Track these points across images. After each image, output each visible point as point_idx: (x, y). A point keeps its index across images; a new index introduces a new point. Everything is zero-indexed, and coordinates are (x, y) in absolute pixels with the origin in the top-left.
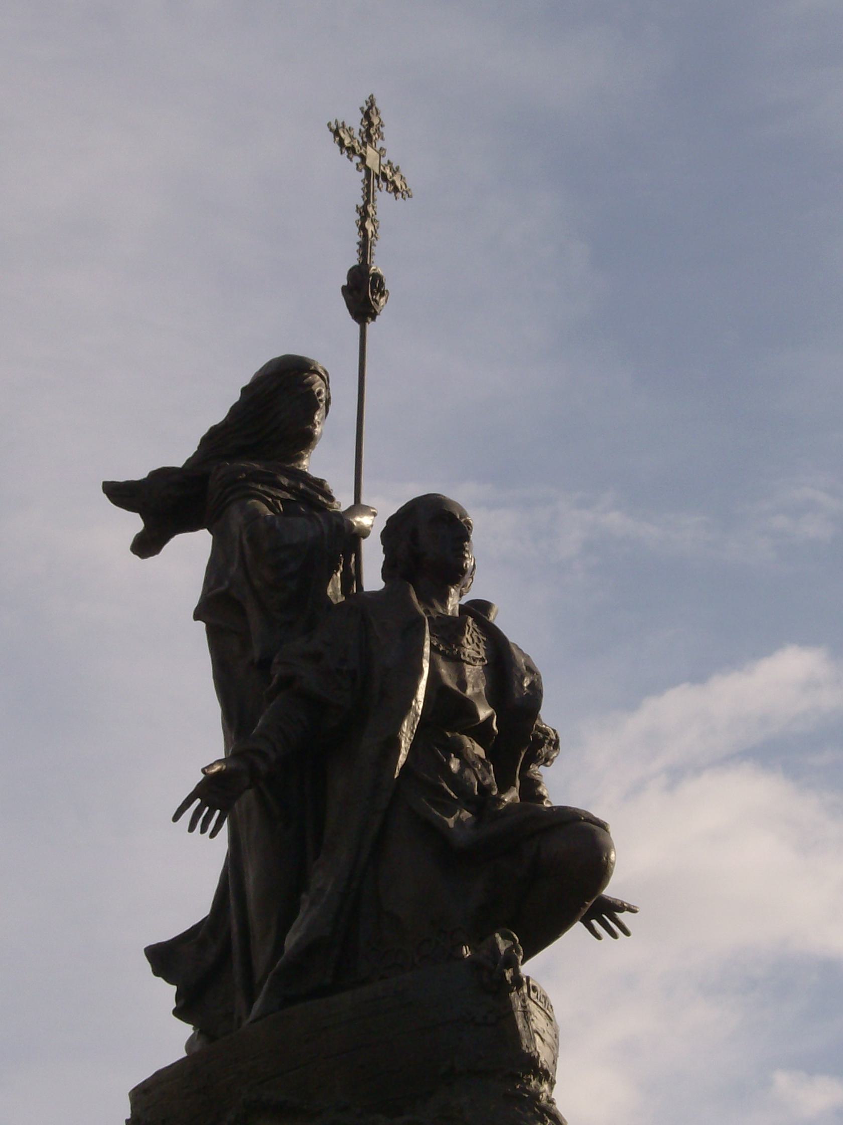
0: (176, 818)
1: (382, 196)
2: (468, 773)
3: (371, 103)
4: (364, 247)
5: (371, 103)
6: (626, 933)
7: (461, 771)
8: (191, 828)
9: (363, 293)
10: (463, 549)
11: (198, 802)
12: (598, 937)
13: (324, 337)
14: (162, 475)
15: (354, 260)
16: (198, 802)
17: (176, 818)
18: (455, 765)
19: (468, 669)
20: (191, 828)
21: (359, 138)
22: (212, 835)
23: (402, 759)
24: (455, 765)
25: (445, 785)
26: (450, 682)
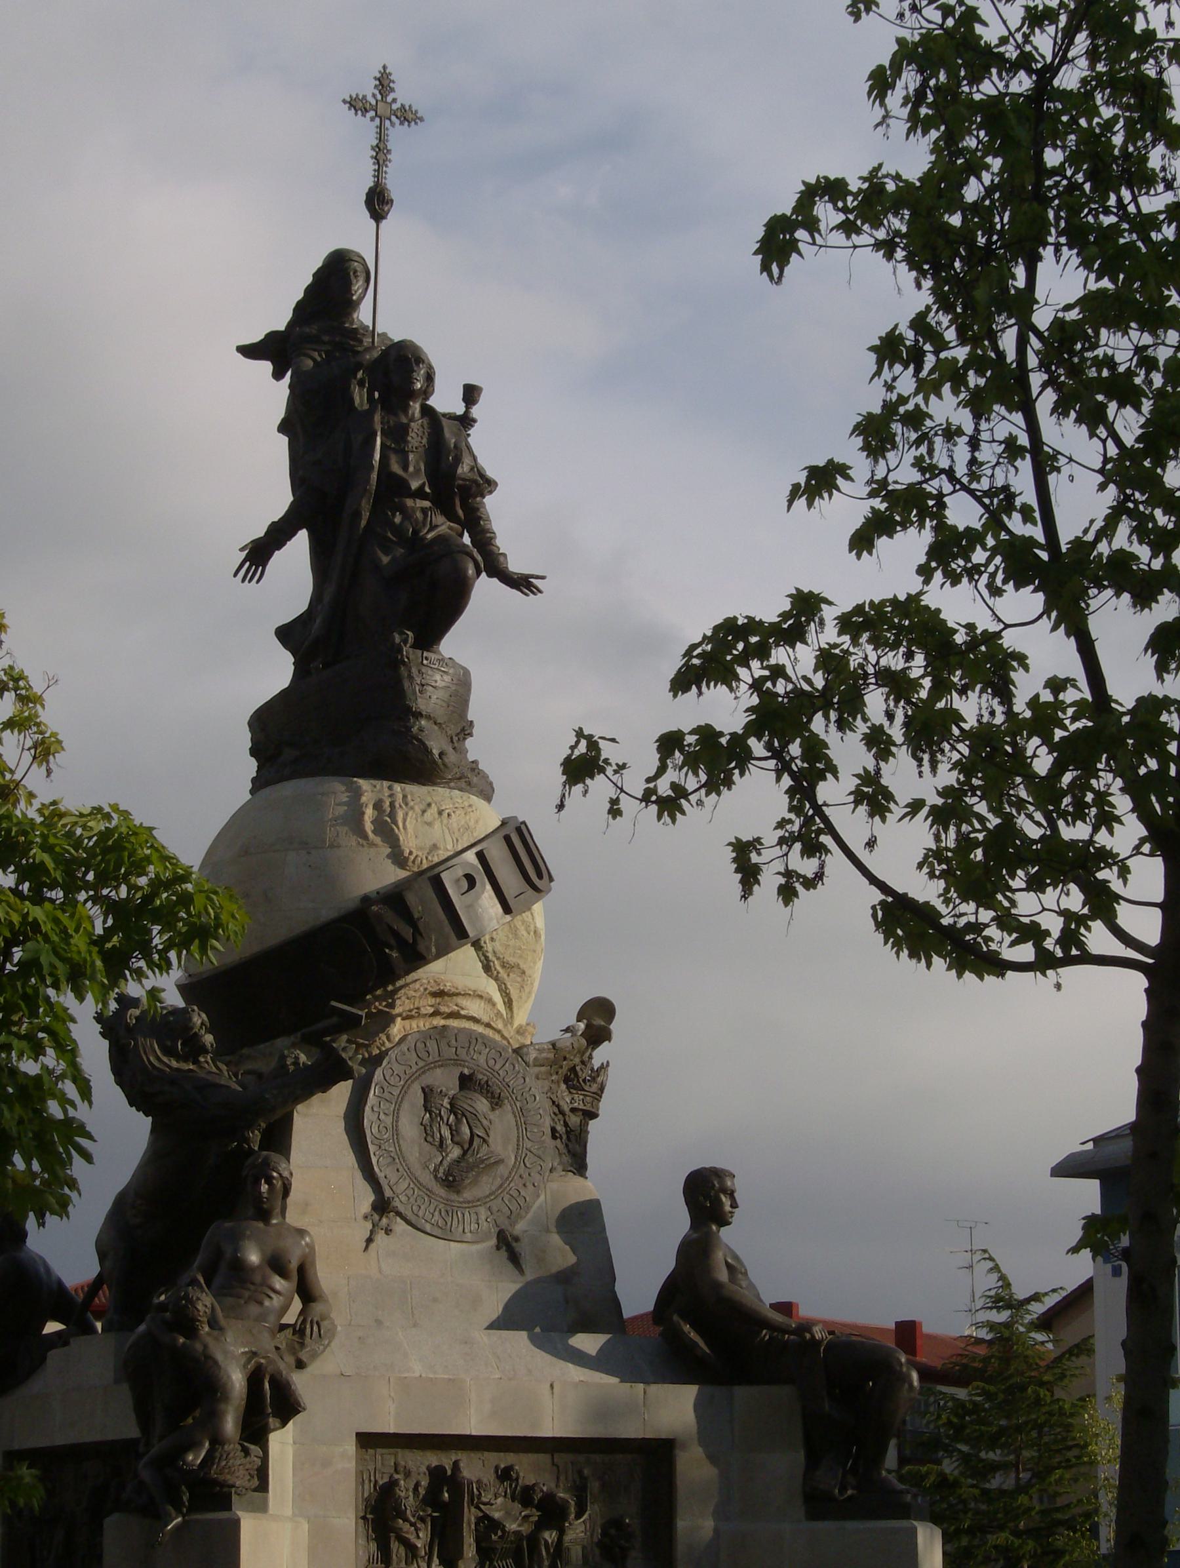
0: (235, 575)
1: (397, 134)
2: (407, 523)
3: (584, 795)
4: (378, 174)
5: (584, 795)
6: (540, 592)
7: (402, 523)
8: (243, 581)
9: (377, 203)
10: (399, 682)
11: (248, 564)
12: (527, 595)
13: (354, 233)
14: (272, 336)
15: (370, 183)
16: (248, 564)
17: (235, 575)
18: (398, 519)
19: (411, 456)
20: (243, 581)
21: (381, 106)
22: (258, 581)
23: (363, 523)
24: (398, 519)
25: (389, 534)
26: (396, 468)
